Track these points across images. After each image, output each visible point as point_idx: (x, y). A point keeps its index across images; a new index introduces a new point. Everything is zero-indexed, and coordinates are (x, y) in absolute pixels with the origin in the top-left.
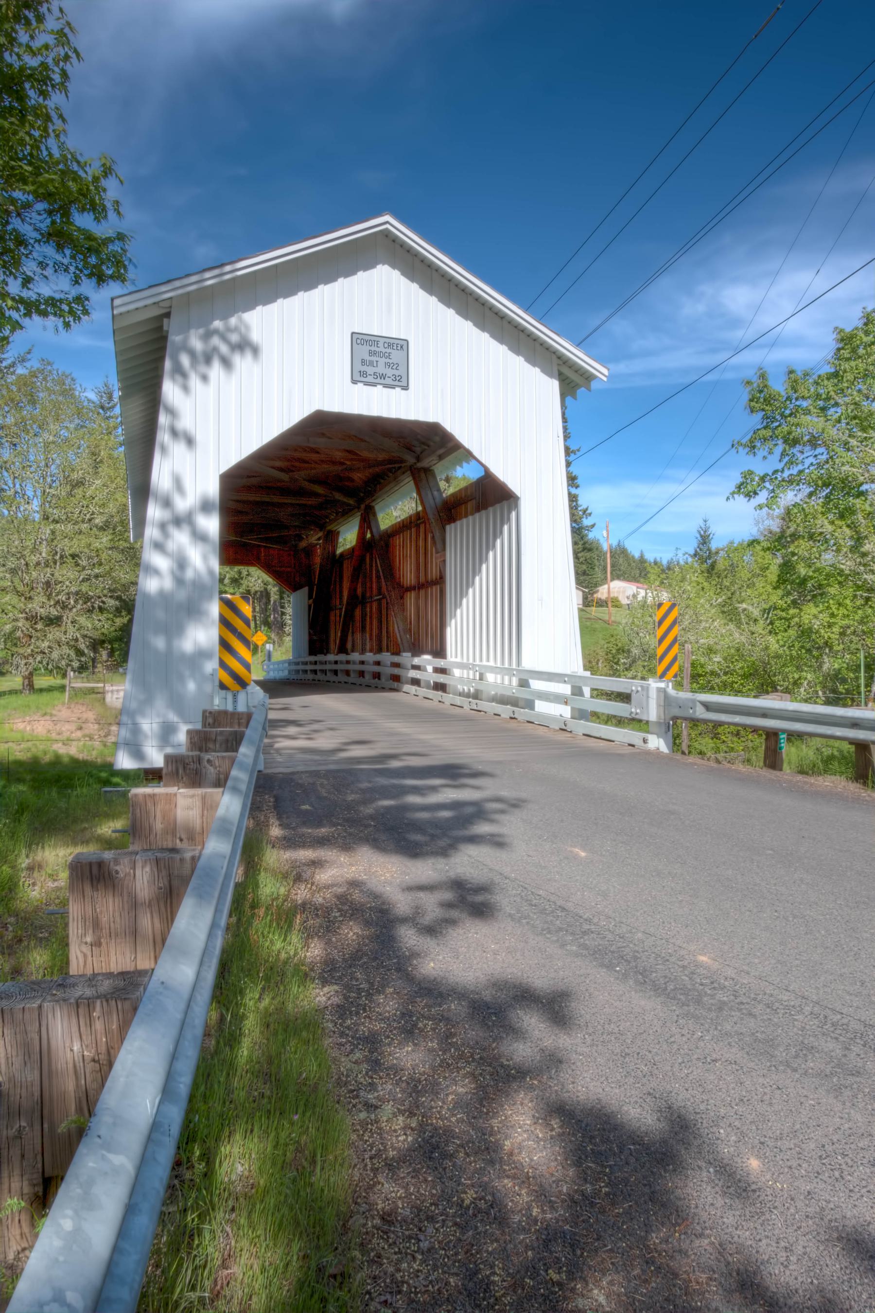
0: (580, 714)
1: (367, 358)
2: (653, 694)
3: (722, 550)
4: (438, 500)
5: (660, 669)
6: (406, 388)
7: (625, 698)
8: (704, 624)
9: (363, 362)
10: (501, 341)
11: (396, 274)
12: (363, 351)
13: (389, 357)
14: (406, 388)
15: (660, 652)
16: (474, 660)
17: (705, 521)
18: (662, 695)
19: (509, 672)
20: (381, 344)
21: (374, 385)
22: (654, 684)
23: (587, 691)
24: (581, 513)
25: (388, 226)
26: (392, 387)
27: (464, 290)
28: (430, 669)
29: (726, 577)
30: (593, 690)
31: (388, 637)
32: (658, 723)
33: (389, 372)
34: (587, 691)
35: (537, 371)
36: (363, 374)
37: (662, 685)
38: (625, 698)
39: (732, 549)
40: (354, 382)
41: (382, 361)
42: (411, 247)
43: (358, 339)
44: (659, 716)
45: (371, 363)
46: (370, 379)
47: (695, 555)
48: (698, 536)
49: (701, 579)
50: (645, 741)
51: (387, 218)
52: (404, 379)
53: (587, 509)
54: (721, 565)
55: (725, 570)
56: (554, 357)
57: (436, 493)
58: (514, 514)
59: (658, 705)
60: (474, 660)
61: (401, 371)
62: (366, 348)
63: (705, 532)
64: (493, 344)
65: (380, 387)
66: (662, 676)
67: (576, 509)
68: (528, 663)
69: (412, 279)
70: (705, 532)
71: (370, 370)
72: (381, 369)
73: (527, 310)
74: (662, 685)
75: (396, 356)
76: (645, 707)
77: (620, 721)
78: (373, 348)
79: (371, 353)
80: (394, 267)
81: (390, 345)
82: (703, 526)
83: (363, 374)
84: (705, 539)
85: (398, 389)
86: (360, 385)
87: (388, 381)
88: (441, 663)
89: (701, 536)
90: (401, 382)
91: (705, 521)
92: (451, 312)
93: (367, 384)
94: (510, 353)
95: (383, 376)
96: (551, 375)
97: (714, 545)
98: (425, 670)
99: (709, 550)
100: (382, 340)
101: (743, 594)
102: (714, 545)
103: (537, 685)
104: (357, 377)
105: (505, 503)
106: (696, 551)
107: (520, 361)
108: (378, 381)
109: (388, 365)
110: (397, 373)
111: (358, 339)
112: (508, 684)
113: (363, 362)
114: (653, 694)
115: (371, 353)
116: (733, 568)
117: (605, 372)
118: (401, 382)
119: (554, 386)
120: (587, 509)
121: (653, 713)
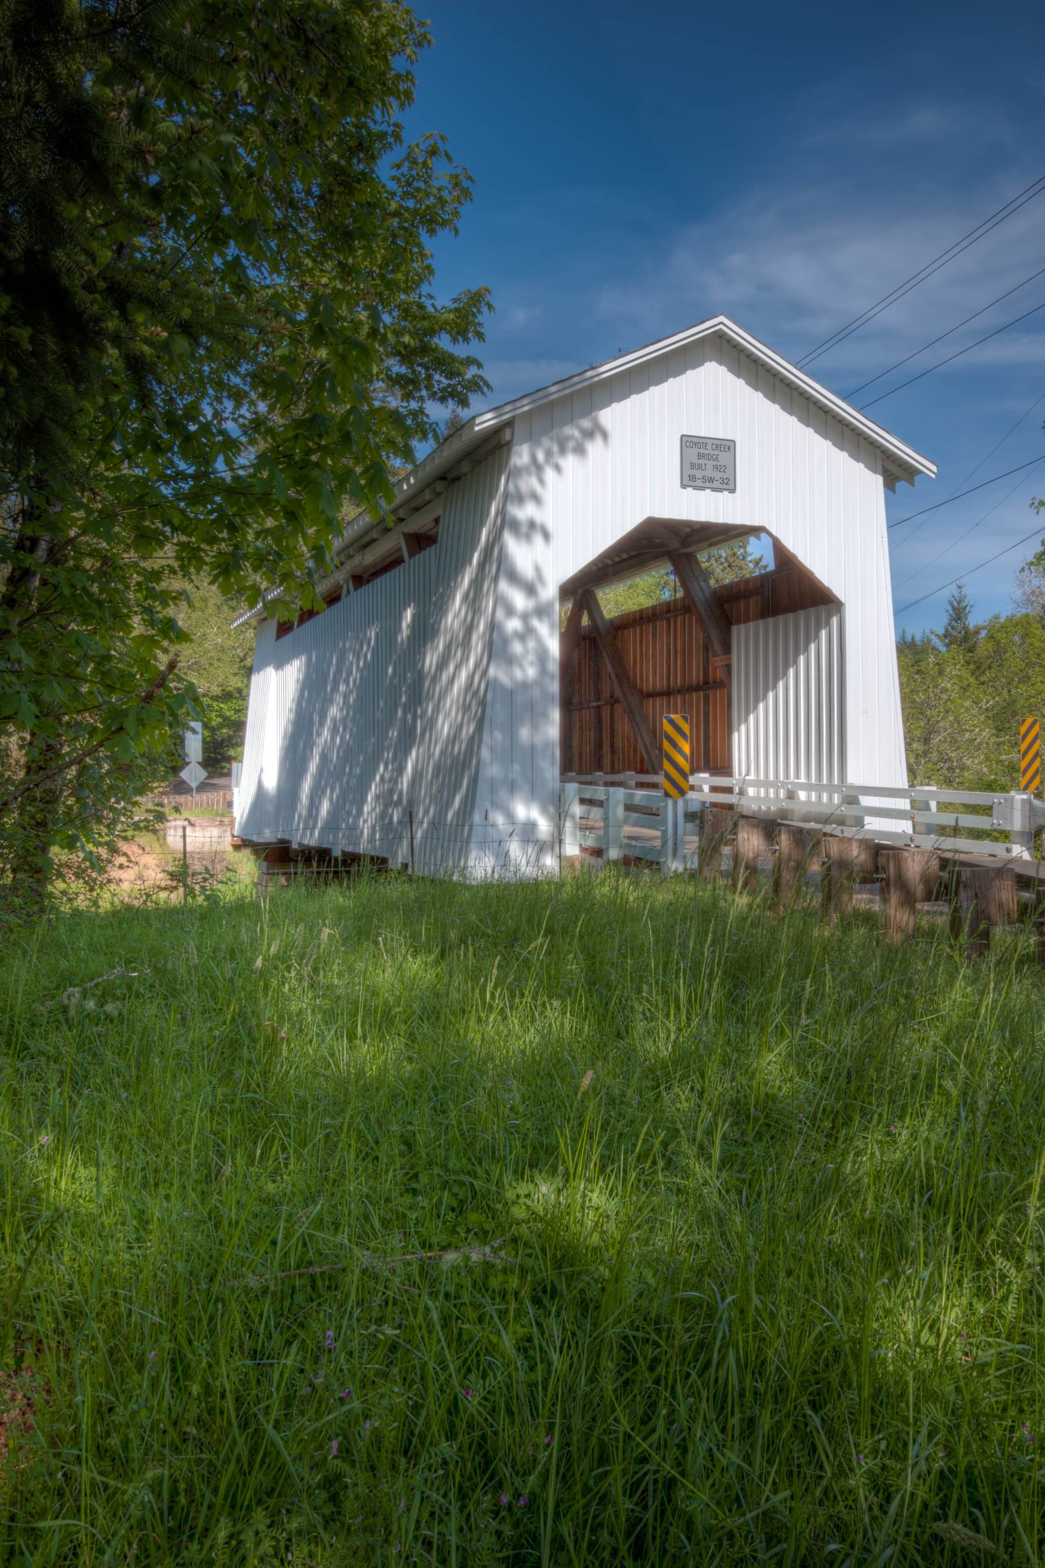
0: (930, 829)
1: (696, 461)
2: (1018, 805)
3: (984, 628)
4: (707, 593)
5: (1023, 782)
6: (733, 491)
7: (987, 810)
8: (967, 735)
9: (692, 466)
10: (825, 437)
11: (722, 370)
12: (692, 454)
13: (717, 459)
14: (733, 491)
15: (1023, 765)
16: (787, 776)
17: (960, 587)
18: (1027, 806)
19: (831, 788)
20: (709, 447)
21: (702, 488)
22: (1019, 797)
23: (933, 805)
24: (751, 565)
25: (721, 327)
26: (720, 490)
27: (789, 385)
28: (706, 788)
29: (990, 667)
30: (938, 803)
31: (613, 752)
32: (1022, 833)
33: (717, 475)
34: (933, 805)
35: (861, 466)
36: (693, 478)
37: (1025, 797)
38: (987, 810)
39: (997, 630)
40: (684, 486)
41: (710, 464)
42: (739, 344)
43: (688, 442)
44: (1023, 825)
45: (699, 467)
46: (699, 483)
47: (945, 636)
48: (949, 608)
49: (965, 673)
50: (1008, 850)
51: (722, 319)
52: (731, 482)
53: (760, 559)
54: (984, 648)
55: (988, 657)
56: (878, 451)
57: (703, 584)
58: (835, 620)
59: (1023, 816)
60: (787, 776)
61: (728, 474)
62: (696, 451)
63: (959, 602)
64: (817, 439)
65: (708, 491)
66: (1026, 788)
67: (744, 558)
68: (856, 776)
69: (738, 375)
70: (959, 602)
71: (699, 474)
72: (709, 472)
73: (859, 410)
74: (1025, 797)
75: (724, 457)
76: (1009, 818)
77: (977, 834)
78: (702, 451)
79: (700, 456)
80: (720, 363)
81: (718, 447)
82: (956, 594)
83: (693, 478)
84: (959, 612)
85: (726, 493)
86: (690, 489)
87: (716, 484)
88: (721, 781)
89: (954, 609)
90: (727, 484)
91: (960, 587)
92: (793, 420)
93: (696, 488)
94: (747, 387)
95: (711, 480)
96: (875, 472)
97: (974, 620)
98: (701, 790)
99: (965, 628)
100: (710, 442)
101: (1013, 691)
102: (974, 620)
103: (866, 801)
104: (686, 482)
105: (823, 609)
106: (947, 630)
107: (844, 456)
108: (707, 484)
109: (716, 467)
110: (724, 475)
111: (688, 442)
112: (831, 801)
113: (692, 466)
114: (1018, 805)
115: (700, 456)
116: (999, 651)
117: (934, 468)
118: (727, 484)
119: (879, 479)
120: (760, 559)
121: (1017, 823)
